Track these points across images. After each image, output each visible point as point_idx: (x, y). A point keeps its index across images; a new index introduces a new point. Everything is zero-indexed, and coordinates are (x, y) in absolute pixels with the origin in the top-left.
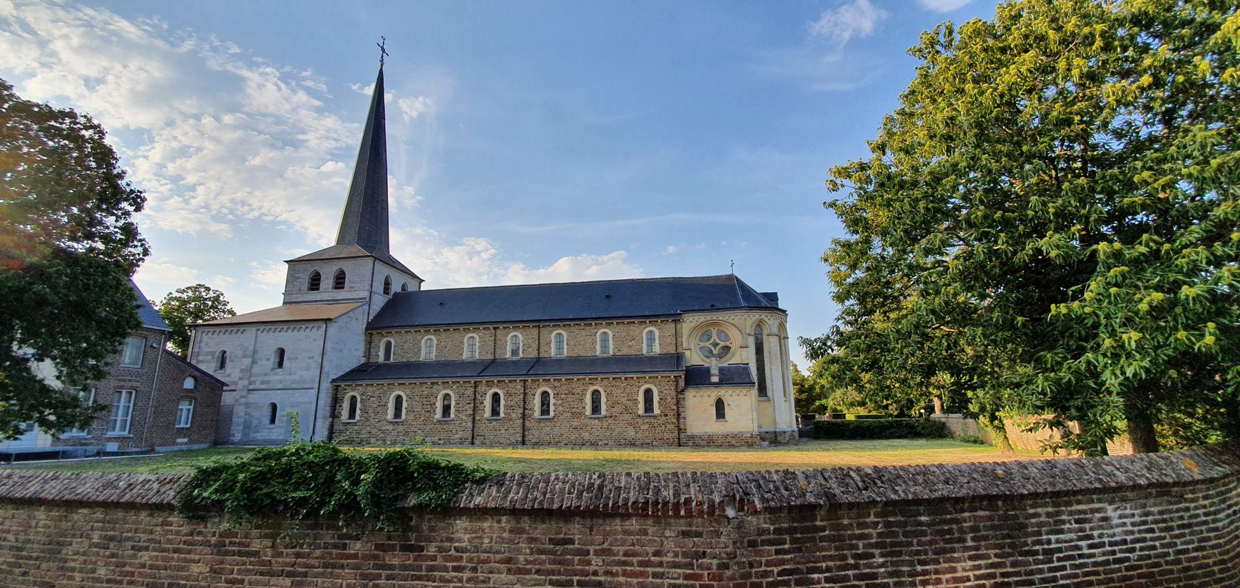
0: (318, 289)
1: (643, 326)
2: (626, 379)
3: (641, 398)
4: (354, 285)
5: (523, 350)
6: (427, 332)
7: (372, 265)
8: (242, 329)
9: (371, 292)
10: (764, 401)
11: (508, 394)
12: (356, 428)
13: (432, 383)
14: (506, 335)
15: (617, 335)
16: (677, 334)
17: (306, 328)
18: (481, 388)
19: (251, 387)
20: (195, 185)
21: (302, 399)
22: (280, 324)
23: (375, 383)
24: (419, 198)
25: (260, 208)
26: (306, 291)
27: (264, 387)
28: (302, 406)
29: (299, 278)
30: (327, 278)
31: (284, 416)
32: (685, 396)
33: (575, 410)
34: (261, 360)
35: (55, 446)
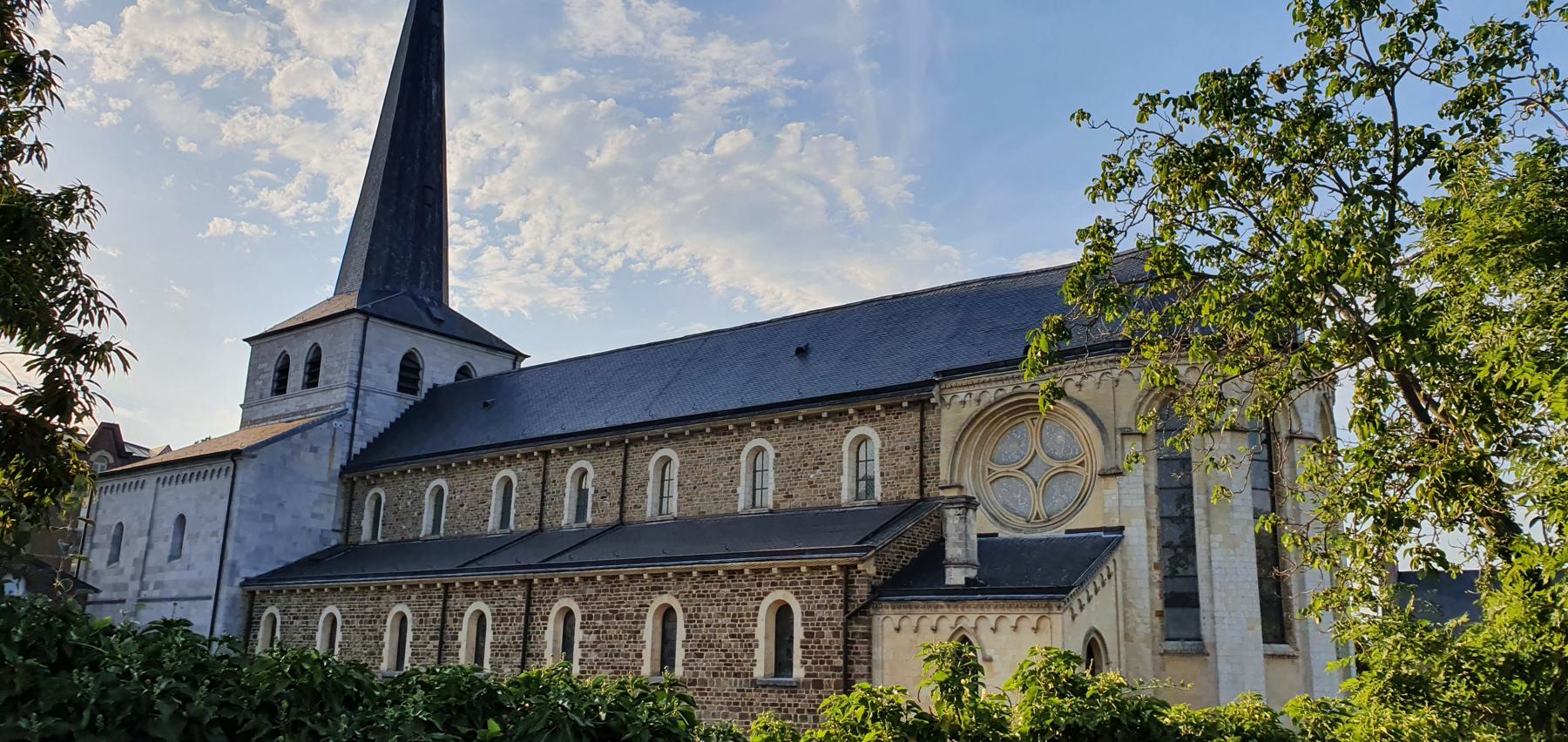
1: (843, 425)
2: (731, 574)
3: (763, 630)
5: (595, 504)
6: (433, 471)
7: (359, 332)
9: (357, 389)
10: (1182, 654)
11: (500, 616)
14: (564, 471)
15: (785, 454)
16: (924, 446)
18: (456, 601)
20: (518, 221)
24: (910, 178)
25: (623, 249)
32: (876, 632)
33: (621, 660)
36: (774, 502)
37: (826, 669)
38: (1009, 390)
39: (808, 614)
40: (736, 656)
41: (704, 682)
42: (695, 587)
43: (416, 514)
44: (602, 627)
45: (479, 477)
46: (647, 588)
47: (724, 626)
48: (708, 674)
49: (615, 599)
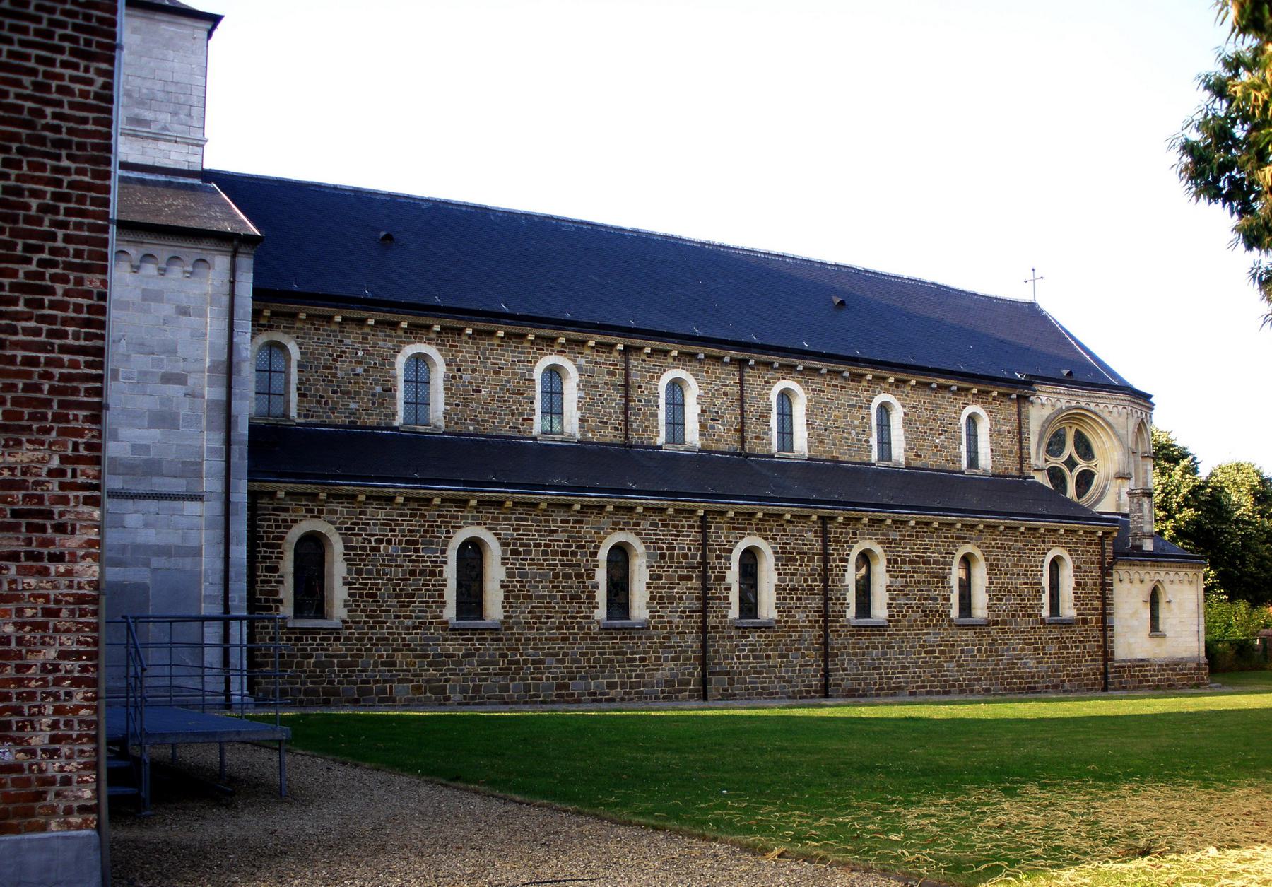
1: (960, 401)
4: (148, 115)
6: (418, 331)
11: (784, 557)
12: (340, 647)
13: (586, 508)
17: (148, 257)
18: (721, 533)
21: (150, 537)
23: (401, 492)
28: (156, 562)
35: (462, 619)
36: (906, 459)
37: (1089, 609)
38: (1073, 404)
39: (1078, 567)
40: (1029, 600)
41: (1004, 622)
42: (994, 540)
43: (378, 389)
44: (909, 572)
45: (383, 343)
46: (952, 537)
47: (1019, 575)
48: (1008, 615)
49: (921, 545)
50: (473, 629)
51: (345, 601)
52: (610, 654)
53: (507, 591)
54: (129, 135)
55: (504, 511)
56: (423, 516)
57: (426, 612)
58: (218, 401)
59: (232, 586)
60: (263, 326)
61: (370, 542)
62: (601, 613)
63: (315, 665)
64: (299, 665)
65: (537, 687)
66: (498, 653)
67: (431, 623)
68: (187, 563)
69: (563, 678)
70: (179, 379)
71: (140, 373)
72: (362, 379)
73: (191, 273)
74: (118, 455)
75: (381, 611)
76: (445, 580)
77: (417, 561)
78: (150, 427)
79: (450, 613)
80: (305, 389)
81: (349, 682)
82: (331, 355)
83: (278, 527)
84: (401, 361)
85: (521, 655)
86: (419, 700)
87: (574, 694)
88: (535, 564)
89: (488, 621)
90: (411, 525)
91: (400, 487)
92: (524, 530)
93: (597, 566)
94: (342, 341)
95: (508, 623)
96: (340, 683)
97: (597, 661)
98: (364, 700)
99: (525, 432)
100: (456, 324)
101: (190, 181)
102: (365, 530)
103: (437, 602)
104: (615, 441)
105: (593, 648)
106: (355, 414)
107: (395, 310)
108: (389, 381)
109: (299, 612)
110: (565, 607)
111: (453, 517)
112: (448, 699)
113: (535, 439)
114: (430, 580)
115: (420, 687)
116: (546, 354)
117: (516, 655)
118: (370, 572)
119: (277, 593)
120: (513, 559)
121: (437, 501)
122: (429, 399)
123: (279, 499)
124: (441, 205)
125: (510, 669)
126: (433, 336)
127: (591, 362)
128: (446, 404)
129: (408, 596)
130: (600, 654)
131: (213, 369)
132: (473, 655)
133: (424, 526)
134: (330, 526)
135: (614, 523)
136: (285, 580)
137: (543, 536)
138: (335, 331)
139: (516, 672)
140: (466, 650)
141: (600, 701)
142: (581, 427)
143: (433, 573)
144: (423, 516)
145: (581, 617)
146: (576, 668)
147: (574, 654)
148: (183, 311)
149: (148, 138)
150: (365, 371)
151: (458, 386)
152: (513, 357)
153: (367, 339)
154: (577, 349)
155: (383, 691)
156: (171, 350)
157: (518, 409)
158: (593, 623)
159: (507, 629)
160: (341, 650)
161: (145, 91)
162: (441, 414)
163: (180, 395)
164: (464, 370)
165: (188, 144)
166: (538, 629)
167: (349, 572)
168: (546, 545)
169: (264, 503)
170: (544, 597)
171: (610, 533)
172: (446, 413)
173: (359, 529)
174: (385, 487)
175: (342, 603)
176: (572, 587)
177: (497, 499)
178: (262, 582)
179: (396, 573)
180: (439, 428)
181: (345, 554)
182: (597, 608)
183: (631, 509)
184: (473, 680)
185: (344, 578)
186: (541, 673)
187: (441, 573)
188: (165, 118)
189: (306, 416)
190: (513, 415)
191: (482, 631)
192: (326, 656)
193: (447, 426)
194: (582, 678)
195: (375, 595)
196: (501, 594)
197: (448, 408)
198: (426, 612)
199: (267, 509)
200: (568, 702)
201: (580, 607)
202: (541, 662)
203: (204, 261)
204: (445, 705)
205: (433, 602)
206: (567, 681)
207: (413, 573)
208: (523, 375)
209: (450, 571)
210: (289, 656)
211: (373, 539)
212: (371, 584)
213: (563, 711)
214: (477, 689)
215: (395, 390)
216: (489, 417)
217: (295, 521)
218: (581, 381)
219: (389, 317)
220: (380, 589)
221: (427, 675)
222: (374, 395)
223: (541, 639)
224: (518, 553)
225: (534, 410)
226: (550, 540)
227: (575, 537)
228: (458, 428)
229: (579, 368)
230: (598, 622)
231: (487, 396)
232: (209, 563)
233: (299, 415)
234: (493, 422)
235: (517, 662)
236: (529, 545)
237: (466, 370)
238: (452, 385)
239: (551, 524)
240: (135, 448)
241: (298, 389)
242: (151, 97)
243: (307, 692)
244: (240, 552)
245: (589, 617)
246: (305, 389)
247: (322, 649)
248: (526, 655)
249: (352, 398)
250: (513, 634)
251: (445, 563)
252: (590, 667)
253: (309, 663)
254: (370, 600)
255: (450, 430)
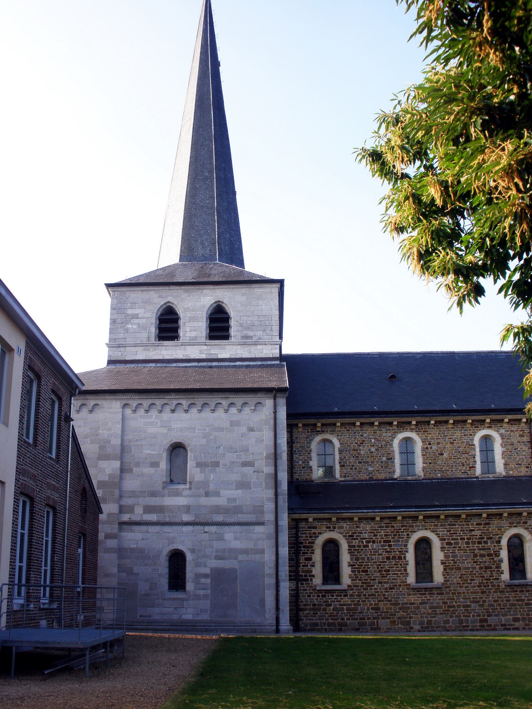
0: (227, 337)
4: (251, 333)
6: (403, 426)
8: (91, 403)
13: (489, 516)
17: (232, 404)
19: (126, 517)
21: (237, 544)
22: (173, 396)
23: (378, 514)
26: (203, 340)
27: (153, 517)
28: (241, 557)
29: (136, 316)
30: (193, 319)
31: (206, 576)
34: (138, 465)
43: (384, 459)
45: (385, 434)
50: (425, 588)
51: (350, 575)
52: (514, 600)
53: (445, 566)
54: (242, 344)
55: (441, 521)
56: (393, 527)
57: (397, 579)
58: (270, 473)
59: (280, 568)
60: (319, 431)
61: (363, 542)
62: (506, 576)
63: (333, 609)
64: (324, 610)
65: (467, 621)
66: (441, 601)
67: (400, 585)
68: (257, 557)
69: (484, 616)
70: (250, 464)
71: (230, 462)
72: (375, 454)
73: (254, 410)
74: (220, 504)
75: (371, 580)
76: (408, 561)
77: (391, 552)
78: (236, 489)
79: (411, 579)
80: (344, 462)
81: (353, 619)
82: (357, 443)
83: (311, 537)
84: (396, 443)
85: (456, 602)
86: (394, 629)
87: (491, 625)
88: (462, 550)
89: (435, 583)
90: (386, 532)
91: (377, 512)
92: (453, 531)
93: (501, 549)
94: (362, 435)
95: (447, 584)
96: (348, 619)
97: (505, 605)
98: (362, 629)
99: (471, 474)
100: (424, 419)
101: (273, 362)
102: (360, 536)
103: (403, 574)
104: (527, 474)
105: (502, 597)
106: (371, 473)
107: (389, 415)
108: (390, 454)
109: (325, 581)
110: (482, 574)
111: (410, 526)
112: (412, 628)
113: (477, 477)
114: (399, 562)
115: (394, 622)
116: (480, 430)
117: (452, 602)
118: (363, 559)
119: (311, 571)
120: (448, 548)
121: (399, 518)
122: (414, 461)
123: (310, 522)
124: (489, 354)
125: (449, 611)
126: (413, 427)
127: (508, 431)
128: (423, 463)
129: (385, 571)
130: (507, 601)
131: (267, 457)
132: (426, 603)
133: (394, 532)
134: (340, 535)
135: (510, 523)
136: (316, 565)
137: (466, 533)
138: (358, 430)
139: (454, 612)
140: (422, 600)
141: (509, 629)
142: (505, 468)
143: (400, 558)
144: (393, 527)
145: (493, 579)
146: (492, 609)
147: (489, 601)
148: (251, 430)
149: (251, 344)
150: (376, 450)
151: (430, 453)
152: (461, 433)
153: (376, 433)
154: (499, 425)
155: (372, 624)
156: (246, 450)
157: (466, 462)
158: (501, 582)
159: (446, 587)
160: (348, 601)
161: (249, 322)
162: (421, 469)
163: (251, 472)
164: (433, 444)
165: (271, 344)
166: (466, 587)
167: (351, 559)
168: (468, 539)
169: (303, 525)
170: (468, 568)
171: (508, 529)
172: (424, 469)
173: (357, 536)
174: (368, 512)
175: (348, 576)
176: (485, 562)
177: (434, 515)
178: (303, 566)
179: (378, 558)
180: (420, 476)
181: (349, 550)
182: (502, 573)
183: (520, 514)
184: (427, 617)
185: (348, 562)
186: (469, 613)
187: (405, 558)
188: (259, 333)
189: (345, 477)
190: (463, 465)
191: (431, 589)
192: (340, 605)
193: (425, 476)
194: (496, 615)
195: (367, 571)
196: (441, 568)
197: (425, 465)
198: (397, 579)
199: (304, 528)
200: (487, 630)
201: (492, 574)
202: (469, 606)
203: (260, 403)
204: (410, 631)
205: (401, 574)
206: (486, 617)
207: (388, 558)
208: (468, 442)
209: (410, 556)
210: (318, 605)
211: (364, 541)
212: (364, 565)
213: (479, 636)
214: (429, 622)
215: (394, 459)
216: (449, 468)
217: (320, 533)
218: (503, 442)
219: (386, 420)
220: (370, 568)
221: (398, 615)
222: (382, 462)
223: (468, 593)
224: (451, 544)
225: (476, 462)
226: (470, 536)
227: (486, 533)
228: (431, 476)
229: (501, 435)
230: (504, 582)
231: (447, 456)
232: (269, 557)
233: (341, 476)
234: (452, 471)
235: (453, 606)
236: (457, 539)
237: (434, 444)
238: (426, 453)
239: (470, 526)
240: (229, 500)
241: (340, 463)
242: (252, 325)
243: (329, 625)
244: (284, 551)
245: (498, 579)
246: (344, 462)
247: (337, 601)
248: (459, 602)
249: (370, 465)
250: (450, 590)
251: (407, 552)
252: (501, 609)
253: (330, 609)
254: (364, 574)
255: (425, 478)
